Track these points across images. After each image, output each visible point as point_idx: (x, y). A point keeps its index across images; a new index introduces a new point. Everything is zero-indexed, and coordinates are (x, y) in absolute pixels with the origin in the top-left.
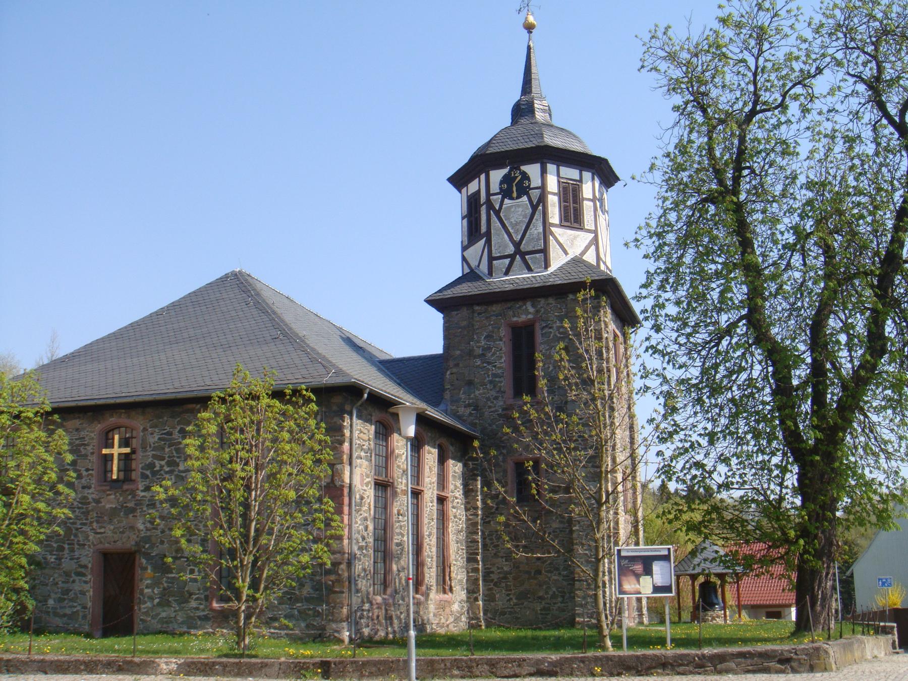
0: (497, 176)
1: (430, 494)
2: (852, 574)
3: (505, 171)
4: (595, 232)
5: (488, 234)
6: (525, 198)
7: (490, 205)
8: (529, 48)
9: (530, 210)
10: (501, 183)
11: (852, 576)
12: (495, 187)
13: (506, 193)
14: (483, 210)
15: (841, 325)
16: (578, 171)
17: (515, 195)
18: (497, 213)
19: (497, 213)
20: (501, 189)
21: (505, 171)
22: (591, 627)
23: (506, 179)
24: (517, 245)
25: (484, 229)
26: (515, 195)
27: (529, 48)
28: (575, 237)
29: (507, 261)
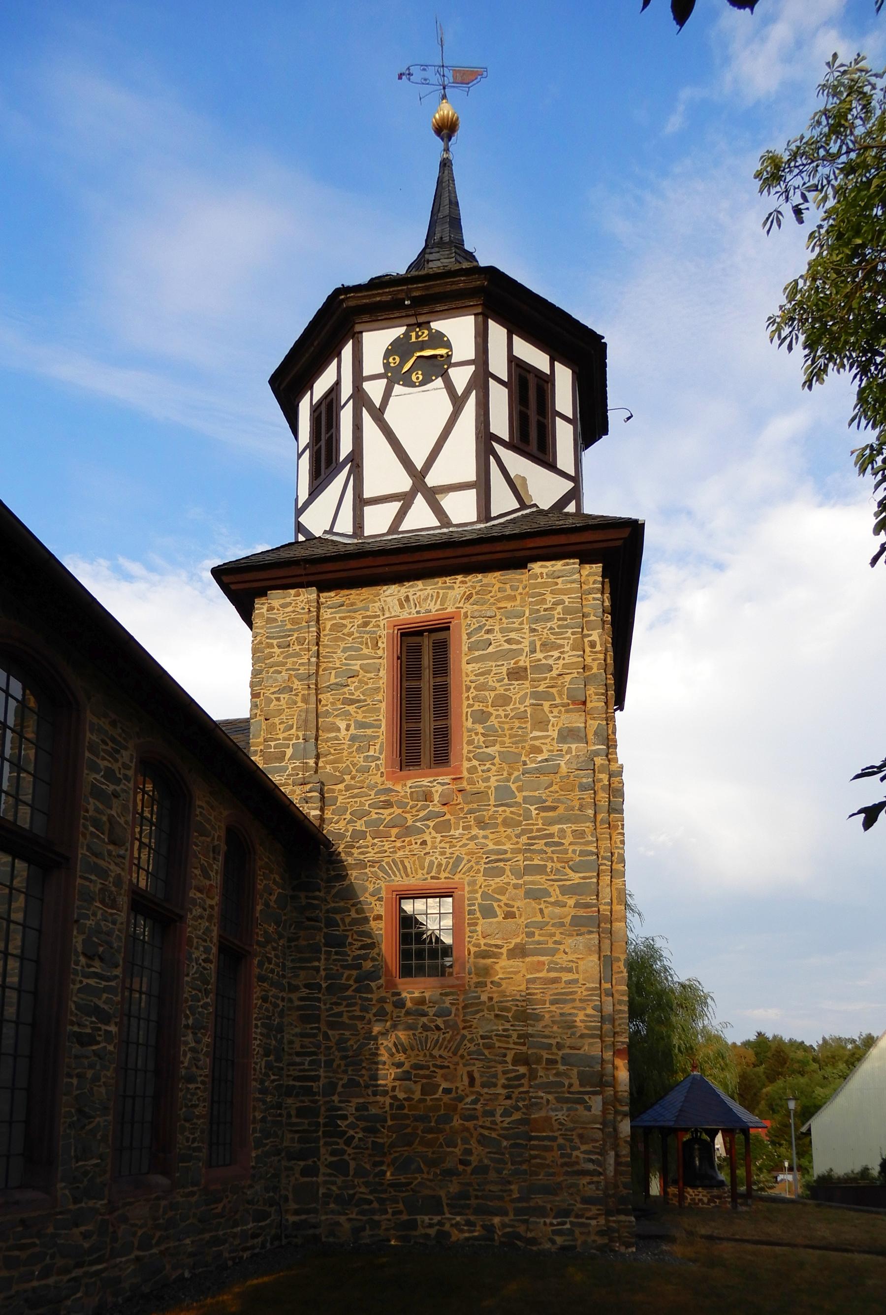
0: (377, 342)
1: (202, 925)
2: (809, 1130)
3: (400, 331)
4: (576, 479)
5: (356, 459)
6: (439, 382)
7: (360, 397)
8: (445, 164)
9: (449, 408)
10: (388, 354)
11: (809, 1133)
12: (373, 363)
13: (394, 376)
14: (346, 417)
15: (836, 152)
16: (474, 478)
17: (442, 351)
18: (378, 415)
19: (378, 415)
20: (386, 365)
21: (400, 331)
22: (579, 656)
23: (398, 348)
24: (418, 476)
25: (346, 447)
26: (442, 351)
27: (445, 164)
28: (485, 590)
29: (396, 506)
